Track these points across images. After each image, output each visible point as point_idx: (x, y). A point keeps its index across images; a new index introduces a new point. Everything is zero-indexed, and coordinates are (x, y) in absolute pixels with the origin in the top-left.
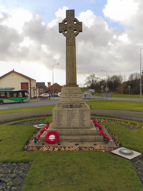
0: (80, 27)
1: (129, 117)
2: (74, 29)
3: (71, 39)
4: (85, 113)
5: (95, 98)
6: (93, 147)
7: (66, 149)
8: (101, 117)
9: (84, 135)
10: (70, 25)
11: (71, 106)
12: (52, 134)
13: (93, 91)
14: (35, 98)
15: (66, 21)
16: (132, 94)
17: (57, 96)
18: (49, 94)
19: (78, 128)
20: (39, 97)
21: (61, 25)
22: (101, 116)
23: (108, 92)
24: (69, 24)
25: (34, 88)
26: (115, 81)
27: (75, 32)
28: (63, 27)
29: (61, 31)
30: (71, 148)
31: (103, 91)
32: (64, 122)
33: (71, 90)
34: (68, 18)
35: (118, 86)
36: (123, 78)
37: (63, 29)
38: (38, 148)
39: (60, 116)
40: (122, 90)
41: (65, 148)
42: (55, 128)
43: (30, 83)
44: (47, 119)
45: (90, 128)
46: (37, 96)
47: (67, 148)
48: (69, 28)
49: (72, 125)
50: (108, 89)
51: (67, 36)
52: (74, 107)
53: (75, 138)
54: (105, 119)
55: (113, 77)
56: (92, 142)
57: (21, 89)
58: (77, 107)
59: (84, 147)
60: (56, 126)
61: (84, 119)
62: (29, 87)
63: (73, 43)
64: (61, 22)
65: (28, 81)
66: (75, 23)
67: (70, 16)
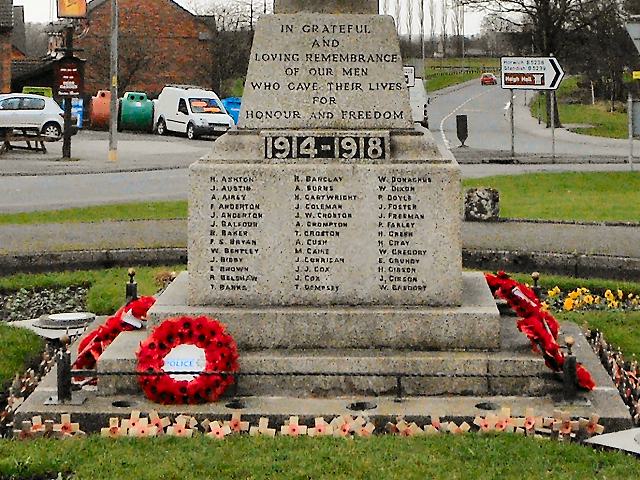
4: (421, 194)
5: (559, 150)
6: (470, 420)
7: (285, 430)
8: (566, 280)
9: (416, 348)
11: (326, 147)
12: (185, 339)
13: (544, 69)
17: (144, 126)
19: (375, 304)
30: (319, 421)
32: (273, 264)
33: (327, 37)
38: (92, 424)
47: (294, 421)
49: (325, 280)
52: (342, 151)
54: (597, 291)
56: (465, 394)
58: (364, 152)
59: (409, 420)
61: (415, 243)
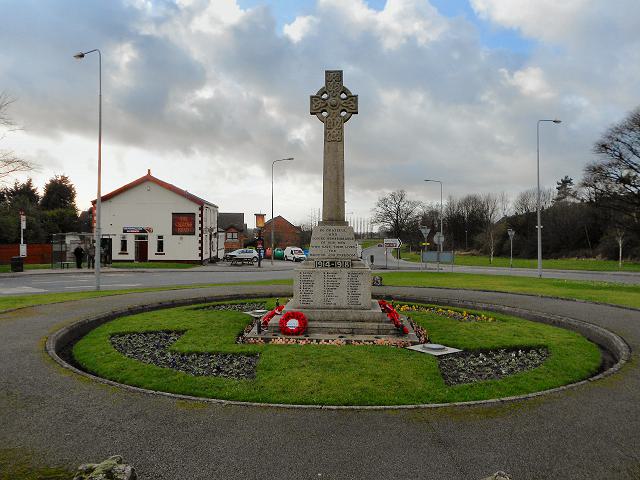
1: (470, 304)
2: (341, 108)
4: (360, 278)
5: (400, 266)
10: (333, 101)
11: (333, 264)
13: (397, 242)
14: (214, 261)
15: (325, 92)
16: (524, 258)
17: (282, 258)
18: (259, 251)
20: (225, 258)
22: (405, 300)
24: (331, 98)
25: (212, 230)
26: (472, 215)
27: (343, 114)
32: (317, 297)
35: (479, 228)
36: (499, 205)
38: (267, 340)
40: (492, 243)
41: (318, 341)
43: (201, 215)
46: (221, 256)
53: (339, 325)
55: (468, 201)
58: (343, 266)
61: (358, 292)
62: (198, 225)
65: (194, 209)
66: (343, 96)
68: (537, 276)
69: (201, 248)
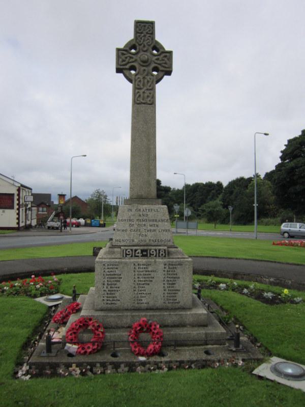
0: (168, 62)
2: (153, 65)
3: (145, 88)
4: (179, 270)
11: (145, 253)
14: (28, 228)
21: (123, 54)
23: (189, 218)
25: (26, 205)
28: (126, 58)
29: (122, 67)
31: (178, 216)
34: (139, 38)
37: (126, 65)
39: (113, 279)
42: (102, 310)
43: (19, 195)
44: (75, 279)
45: (190, 309)
48: (141, 63)
49: (144, 300)
50: (190, 213)
51: (135, 80)
52: (150, 254)
57: (12, 207)
58: (158, 254)
60: (102, 305)
61: (177, 287)
62: (16, 202)
63: (149, 99)
64: (122, 46)
67: (145, 36)
68: (254, 238)
69: (18, 219)
